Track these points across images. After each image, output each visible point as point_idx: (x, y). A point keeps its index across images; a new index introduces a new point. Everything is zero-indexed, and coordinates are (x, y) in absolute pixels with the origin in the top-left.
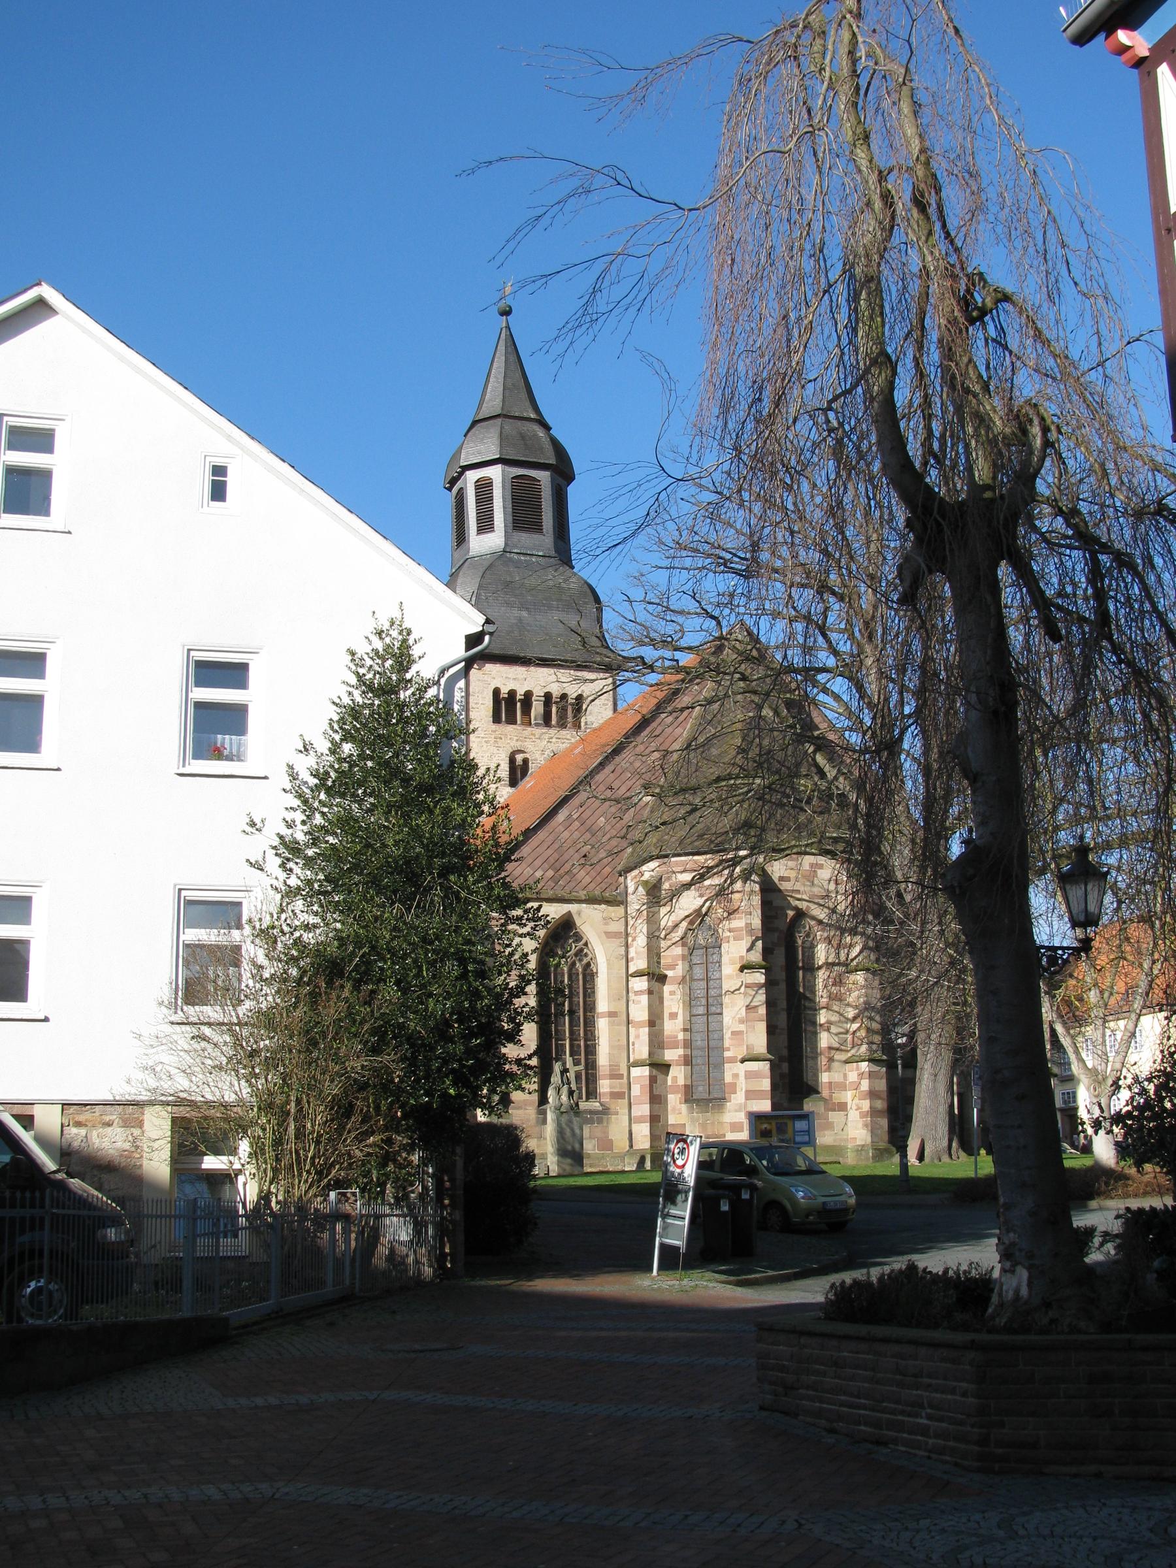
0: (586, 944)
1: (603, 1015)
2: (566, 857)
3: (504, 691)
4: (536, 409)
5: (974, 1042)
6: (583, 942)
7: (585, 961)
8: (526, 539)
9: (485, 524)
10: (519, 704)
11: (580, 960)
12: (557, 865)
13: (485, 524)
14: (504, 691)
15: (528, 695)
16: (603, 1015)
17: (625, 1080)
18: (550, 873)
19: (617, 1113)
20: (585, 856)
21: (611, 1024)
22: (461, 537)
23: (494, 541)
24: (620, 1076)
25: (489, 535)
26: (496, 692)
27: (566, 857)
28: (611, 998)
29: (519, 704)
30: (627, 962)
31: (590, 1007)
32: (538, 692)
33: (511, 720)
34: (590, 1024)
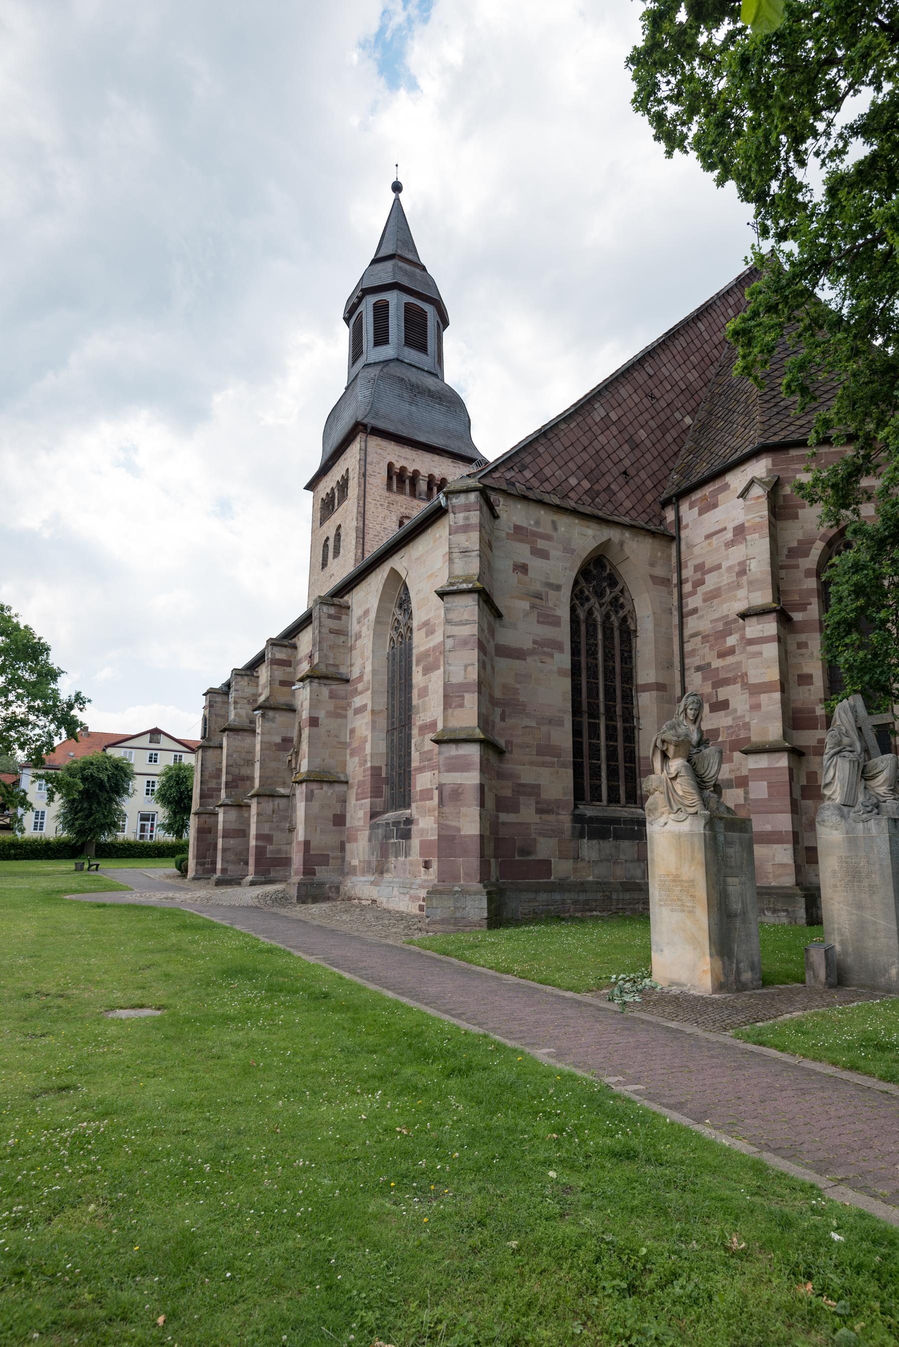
1: (647, 688)
3: (398, 466)
6: (619, 587)
7: (621, 614)
9: (381, 339)
10: (407, 481)
11: (617, 612)
13: (381, 339)
14: (398, 466)
15: (416, 473)
16: (647, 688)
25: (384, 347)
26: (390, 466)
29: (407, 481)
30: (682, 617)
31: (628, 676)
32: (424, 472)
33: (401, 490)
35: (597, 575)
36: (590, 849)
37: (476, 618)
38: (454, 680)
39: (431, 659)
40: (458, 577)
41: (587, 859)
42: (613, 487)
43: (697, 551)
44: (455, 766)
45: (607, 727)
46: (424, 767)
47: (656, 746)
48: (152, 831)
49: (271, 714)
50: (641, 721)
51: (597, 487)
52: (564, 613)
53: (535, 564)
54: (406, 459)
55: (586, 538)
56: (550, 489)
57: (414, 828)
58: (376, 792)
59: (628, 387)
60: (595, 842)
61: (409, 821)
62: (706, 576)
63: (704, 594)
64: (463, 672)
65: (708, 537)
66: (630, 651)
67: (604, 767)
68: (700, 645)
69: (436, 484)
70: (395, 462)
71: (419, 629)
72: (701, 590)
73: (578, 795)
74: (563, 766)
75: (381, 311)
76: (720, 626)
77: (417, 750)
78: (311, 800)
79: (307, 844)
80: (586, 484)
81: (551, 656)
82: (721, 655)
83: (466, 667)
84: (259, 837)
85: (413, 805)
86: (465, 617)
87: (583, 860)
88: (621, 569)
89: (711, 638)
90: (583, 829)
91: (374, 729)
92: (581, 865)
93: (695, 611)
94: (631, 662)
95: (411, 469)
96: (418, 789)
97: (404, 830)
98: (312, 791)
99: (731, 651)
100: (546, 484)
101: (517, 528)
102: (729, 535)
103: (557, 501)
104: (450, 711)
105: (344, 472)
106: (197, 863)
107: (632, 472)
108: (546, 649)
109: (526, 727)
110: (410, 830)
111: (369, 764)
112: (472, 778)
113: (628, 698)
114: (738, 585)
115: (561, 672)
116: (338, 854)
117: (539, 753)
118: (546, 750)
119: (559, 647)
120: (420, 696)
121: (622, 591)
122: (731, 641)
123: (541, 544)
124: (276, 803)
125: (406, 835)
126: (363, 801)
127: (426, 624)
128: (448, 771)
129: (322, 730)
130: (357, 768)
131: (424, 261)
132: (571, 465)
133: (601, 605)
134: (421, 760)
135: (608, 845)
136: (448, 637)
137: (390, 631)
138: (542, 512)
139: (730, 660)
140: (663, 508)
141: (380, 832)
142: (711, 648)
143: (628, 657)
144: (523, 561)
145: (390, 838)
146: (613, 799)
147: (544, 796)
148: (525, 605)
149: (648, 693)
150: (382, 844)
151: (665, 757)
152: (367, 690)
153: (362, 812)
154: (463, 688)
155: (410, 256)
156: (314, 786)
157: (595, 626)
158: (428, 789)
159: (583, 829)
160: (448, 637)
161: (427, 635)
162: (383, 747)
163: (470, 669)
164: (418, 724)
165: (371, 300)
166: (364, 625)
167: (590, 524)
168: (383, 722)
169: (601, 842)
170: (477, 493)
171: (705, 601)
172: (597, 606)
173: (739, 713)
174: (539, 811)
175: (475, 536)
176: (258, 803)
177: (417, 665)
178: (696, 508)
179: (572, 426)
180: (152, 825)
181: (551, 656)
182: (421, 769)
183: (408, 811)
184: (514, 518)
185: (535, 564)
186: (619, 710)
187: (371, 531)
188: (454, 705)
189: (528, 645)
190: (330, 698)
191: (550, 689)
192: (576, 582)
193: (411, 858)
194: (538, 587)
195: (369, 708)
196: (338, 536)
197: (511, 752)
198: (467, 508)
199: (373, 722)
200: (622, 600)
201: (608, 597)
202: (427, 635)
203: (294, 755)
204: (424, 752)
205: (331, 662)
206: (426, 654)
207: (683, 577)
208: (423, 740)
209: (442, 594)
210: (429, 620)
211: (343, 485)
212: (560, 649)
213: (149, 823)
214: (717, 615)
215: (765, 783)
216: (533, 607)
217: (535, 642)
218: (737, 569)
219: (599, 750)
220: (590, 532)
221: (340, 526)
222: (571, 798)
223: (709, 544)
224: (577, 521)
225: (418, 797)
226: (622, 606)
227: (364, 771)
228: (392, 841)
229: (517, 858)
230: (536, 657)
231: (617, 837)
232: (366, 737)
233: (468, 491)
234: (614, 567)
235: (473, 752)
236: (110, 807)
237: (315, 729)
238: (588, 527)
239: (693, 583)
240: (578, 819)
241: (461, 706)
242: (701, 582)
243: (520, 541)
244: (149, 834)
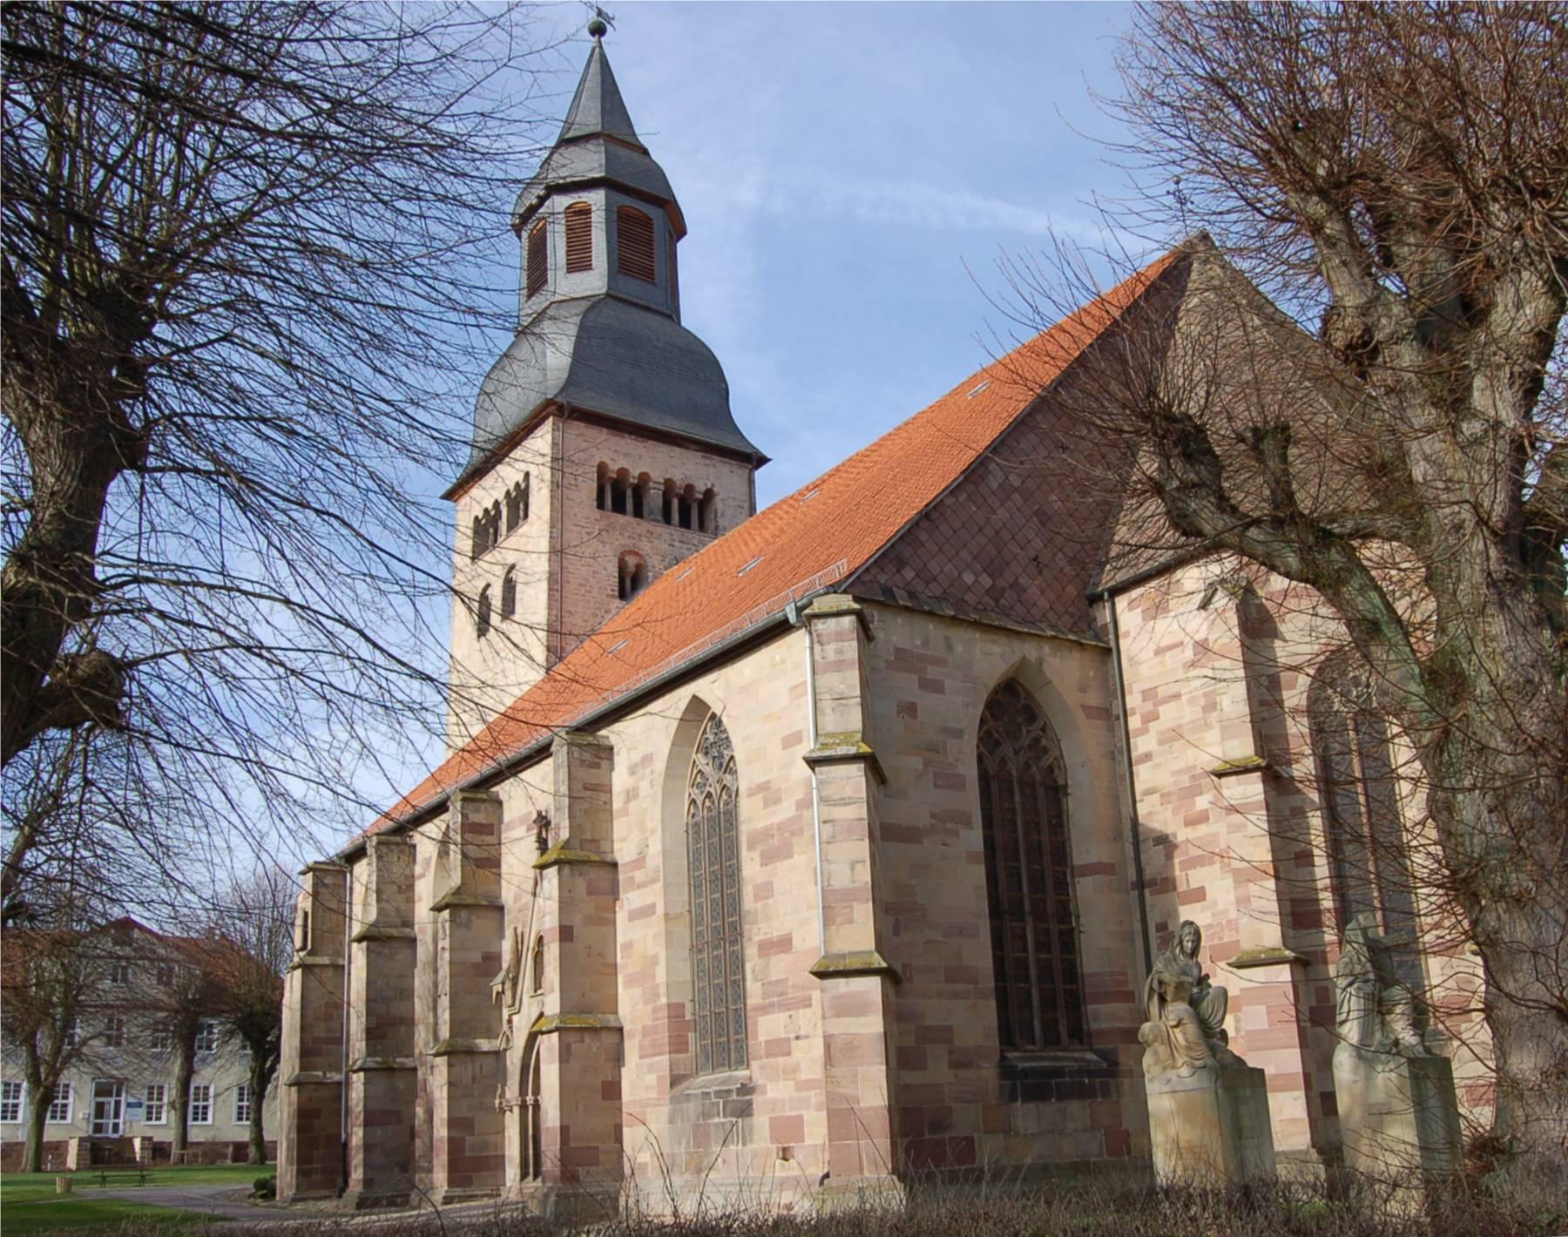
7: (1045, 762)
15: (644, 478)
16: (1089, 870)
25: (586, 273)
26: (602, 469)
33: (619, 507)
35: (1013, 708)
36: (1025, 1115)
37: (864, 795)
39: (775, 841)
40: (832, 735)
41: (1022, 1131)
42: (1021, 581)
43: (1144, 670)
44: (843, 1008)
45: (1036, 932)
46: (772, 1005)
47: (1151, 989)
48: (117, 1115)
49: (464, 914)
50: (1082, 920)
51: (1001, 583)
52: (969, 770)
53: (926, 701)
54: (626, 455)
55: (990, 659)
56: (938, 593)
57: (757, 1099)
58: (678, 1045)
59: (1032, 437)
60: (1031, 1105)
61: (746, 1089)
62: (1161, 709)
63: (1160, 733)
64: (848, 873)
65: (1159, 652)
67: (1035, 992)
68: (1158, 808)
69: (677, 495)
70: (609, 462)
71: (751, 795)
72: (1154, 727)
73: (1008, 1034)
75: (579, 217)
76: (1185, 781)
77: (756, 979)
79: (564, 1130)
80: (986, 581)
82: (1190, 822)
83: (853, 865)
84: (452, 1123)
85: (755, 1064)
86: (848, 793)
87: (1017, 1133)
88: (1040, 697)
89: (1174, 798)
91: (669, 943)
93: (1148, 757)
94: (1062, 833)
95: (635, 472)
96: (762, 1038)
97: (741, 1104)
98: (569, 1046)
99: (1203, 818)
100: (933, 585)
101: (899, 652)
102: (1189, 654)
104: (833, 928)
105: (520, 477)
106: (298, 1172)
108: (949, 825)
109: (929, 942)
110: (750, 1103)
111: (664, 1000)
112: (874, 1024)
113: (1062, 886)
114: (1206, 724)
115: (971, 858)
117: (950, 979)
118: (957, 975)
120: (757, 897)
121: (1043, 729)
122: (1202, 802)
123: (932, 672)
124: (477, 1064)
125: (745, 1111)
126: (656, 1059)
127: (764, 787)
128: (837, 1016)
130: (640, 1006)
131: (644, 140)
132: (964, 554)
133: (1016, 753)
134: (765, 995)
135: (1050, 1108)
136: (825, 822)
137: (688, 790)
138: (931, 626)
139: (1203, 830)
140: (1091, 605)
141: (692, 1107)
142: (1175, 812)
144: (910, 699)
145: (710, 1116)
146: (1051, 1039)
147: (958, 1042)
148: (916, 763)
149: (1089, 879)
150: (696, 1127)
151: (1163, 1000)
152: (654, 881)
153: (654, 1076)
154: (850, 895)
155: (628, 139)
156: (572, 1037)
157: (1011, 783)
158: (780, 1040)
159: (1014, 1087)
160: (825, 822)
161: (766, 805)
162: (685, 972)
163: (859, 867)
164: (756, 939)
165: (561, 202)
166: (643, 778)
167: (996, 637)
168: (684, 933)
169: (1041, 1105)
170: (853, 618)
171: (1161, 743)
173: (1221, 906)
174: (956, 1065)
175: (854, 676)
176: (450, 1065)
177: (750, 848)
178: (1139, 610)
179: (961, 499)
180: (118, 1104)
181: (956, 834)
182: (765, 1009)
183: (742, 1073)
184: (895, 638)
185: (926, 701)
186: (1051, 908)
187: (571, 578)
188: (839, 920)
189: (924, 821)
190: (589, 894)
191: (962, 885)
192: (982, 721)
193: (754, 1146)
195: (660, 910)
196: (509, 586)
197: (910, 980)
198: (839, 636)
199: (668, 933)
200: (1044, 742)
201: (1025, 741)
202: (766, 805)
203: (508, 985)
204: (771, 983)
205: (588, 837)
206: (766, 834)
207: (1129, 706)
208: (767, 965)
209: (813, 763)
210: (768, 782)
211: (519, 500)
212: (968, 824)
213: (112, 1100)
214: (1180, 765)
215: (1263, 1009)
216: (926, 764)
217: (933, 815)
218: (1202, 702)
219: (1027, 968)
220: (997, 649)
222: (995, 1043)
223: (1161, 663)
224: (978, 635)
225: (763, 1052)
226: (1045, 750)
227: (654, 1010)
228: (716, 1120)
229: (927, 1136)
231: (1062, 1097)
232: (655, 956)
234: (1029, 695)
235: (872, 987)
237: (567, 945)
238: (993, 642)
239: (1142, 716)
240: (1007, 1071)
242: (1155, 717)
244: (112, 1121)
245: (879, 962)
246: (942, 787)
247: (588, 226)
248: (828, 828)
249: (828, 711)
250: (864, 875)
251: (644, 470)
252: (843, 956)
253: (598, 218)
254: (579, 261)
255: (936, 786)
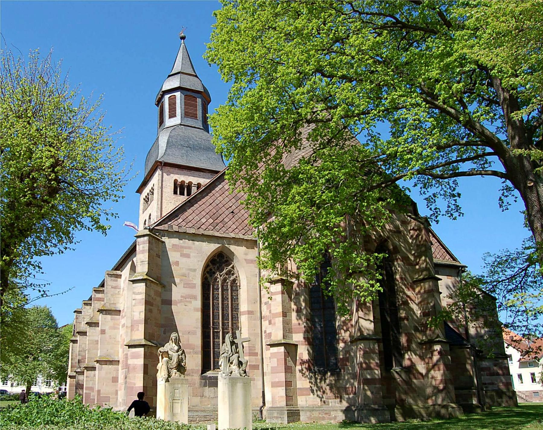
0: (233, 267)
1: (244, 313)
2: (220, 212)
4: (194, 71)
5: (311, 352)
8: (190, 122)
9: (172, 115)
12: (215, 217)
16: (244, 313)
17: (259, 357)
18: (211, 221)
19: (254, 380)
20: (232, 212)
21: (250, 319)
22: (162, 122)
23: (177, 120)
24: (256, 354)
25: (174, 118)
27: (220, 212)
28: (250, 301)
29: (186, 189)
31: (235, 308)
33: (182, 194)
34: (235, 318)
38: (135, 319)
41: (208, 396)
66: (237, 295)
70: (178, 179)
74: (196, 353)
78: (101, 370)
81: (191, 302)
86: (140, 291)
90: (206, 382)
92: (204, 399)
95: (187, 182)
103: (192, 231)
105: (152, 186)
107: (236, 211)
108: (187, 299)
116: (114, 396)
119: (195, 298)
129: (107, 335)
133: (221, 276)
143: (235, 299)
154: (138, 322)
159: (206, 382)
172: (219, 276)
175: (147, 255)
181: (191, 302)
194: (184, 271)
205: (112, 302)
215: (276, 359)
217: (182, 297)
221: (150, 215)
230: (183, 303)
233: (144, 236)
236: (313, 333)
241: (138, 330)
243: (175, 251)
245: (143, 342)
246: (186, 287)
247: (175, 103)
248: (134, 301)
249: (139, 266)
250: (143, 316)
251: (190, 181)
252: (135, 340)
253: (178, 102)
254: (172, 115)
255: (184, 287)
